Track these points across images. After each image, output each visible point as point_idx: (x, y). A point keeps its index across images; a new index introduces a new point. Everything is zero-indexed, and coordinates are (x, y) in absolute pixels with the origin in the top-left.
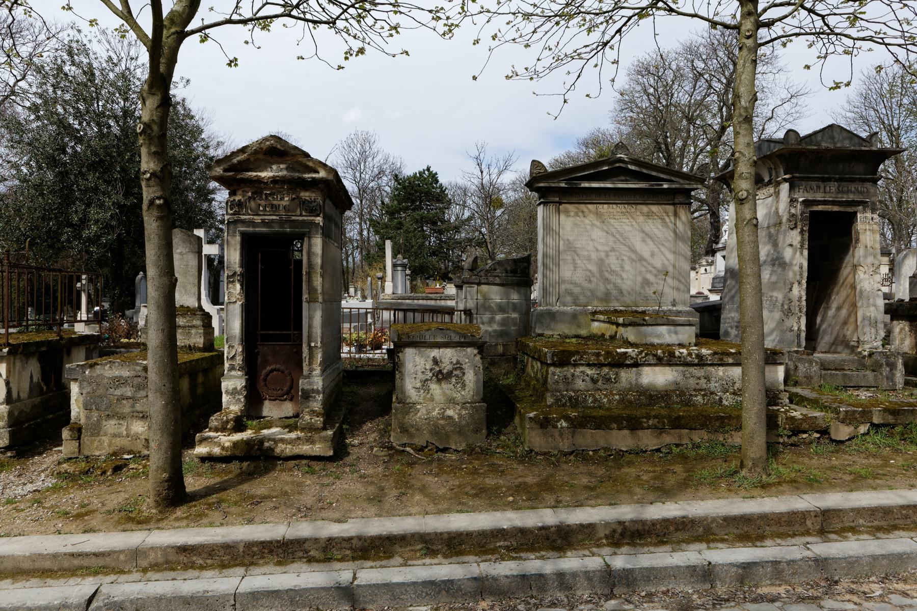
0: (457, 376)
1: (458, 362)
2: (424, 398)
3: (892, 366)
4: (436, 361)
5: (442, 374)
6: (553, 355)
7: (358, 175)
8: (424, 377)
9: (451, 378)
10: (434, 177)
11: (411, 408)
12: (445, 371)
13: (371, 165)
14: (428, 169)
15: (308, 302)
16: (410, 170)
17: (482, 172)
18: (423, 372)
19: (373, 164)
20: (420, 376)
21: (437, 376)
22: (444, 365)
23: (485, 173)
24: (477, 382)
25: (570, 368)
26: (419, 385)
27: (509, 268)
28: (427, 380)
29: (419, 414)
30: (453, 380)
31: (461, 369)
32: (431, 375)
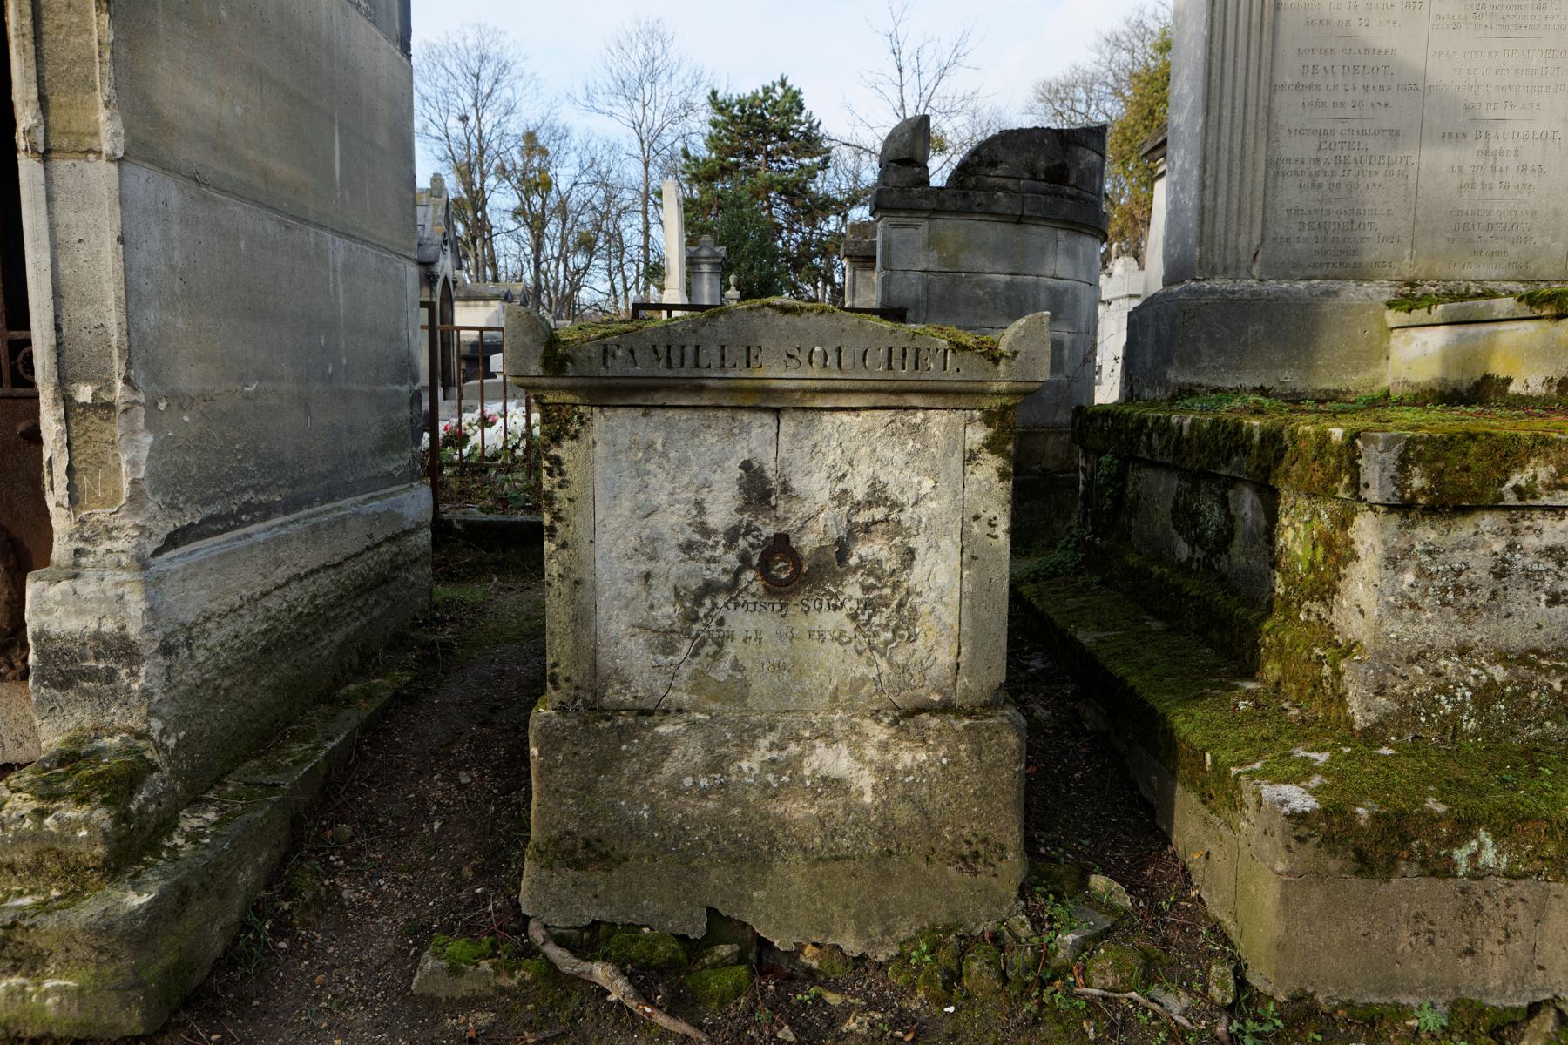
0: (871, 568)
1: (877, 496)
2: (699, 683)
3: (530, 510)
4: (758, 489)
5: (793, 556)
6: (1404, 463)
7: (639, 112)
8: (695, 573)
9: (838, 579)
10: (795, 102)
11: (623, 734)
12: (808, 543)
13: (666, 89)
14: (783, 84)
15: (46, 156)
16: (742, 84)
17: (900, 70)
18: (688, 547)
19: (667, 94)
20: (674, 568)
21: (764, 568)
22: (806, 509)
23: (907, 73)
24: (972, 602)
25: (1487, 521)
26: (667, 612)
27: (1042, 164)
28: (710, 589)
29: (669, 768)
30: (852, 589)
31: (895, 529)
32: (732, 560)
